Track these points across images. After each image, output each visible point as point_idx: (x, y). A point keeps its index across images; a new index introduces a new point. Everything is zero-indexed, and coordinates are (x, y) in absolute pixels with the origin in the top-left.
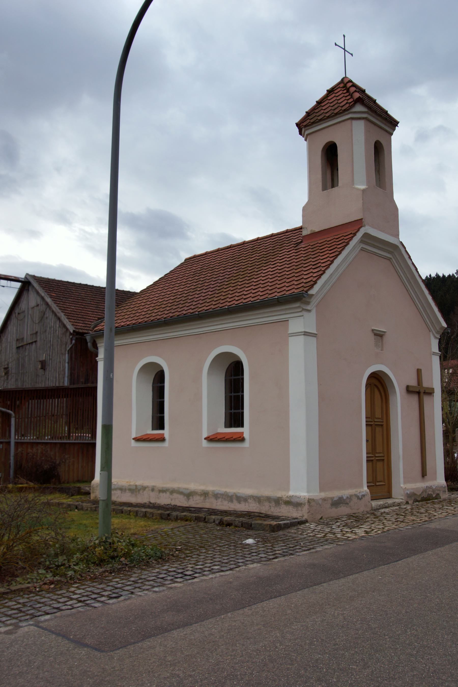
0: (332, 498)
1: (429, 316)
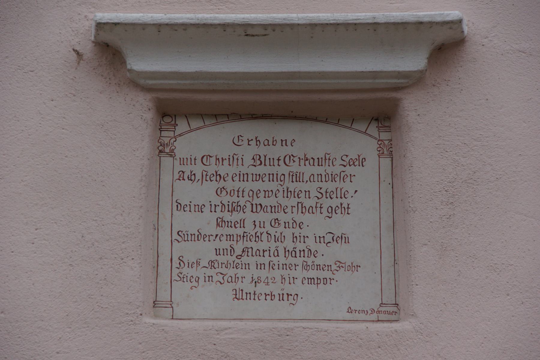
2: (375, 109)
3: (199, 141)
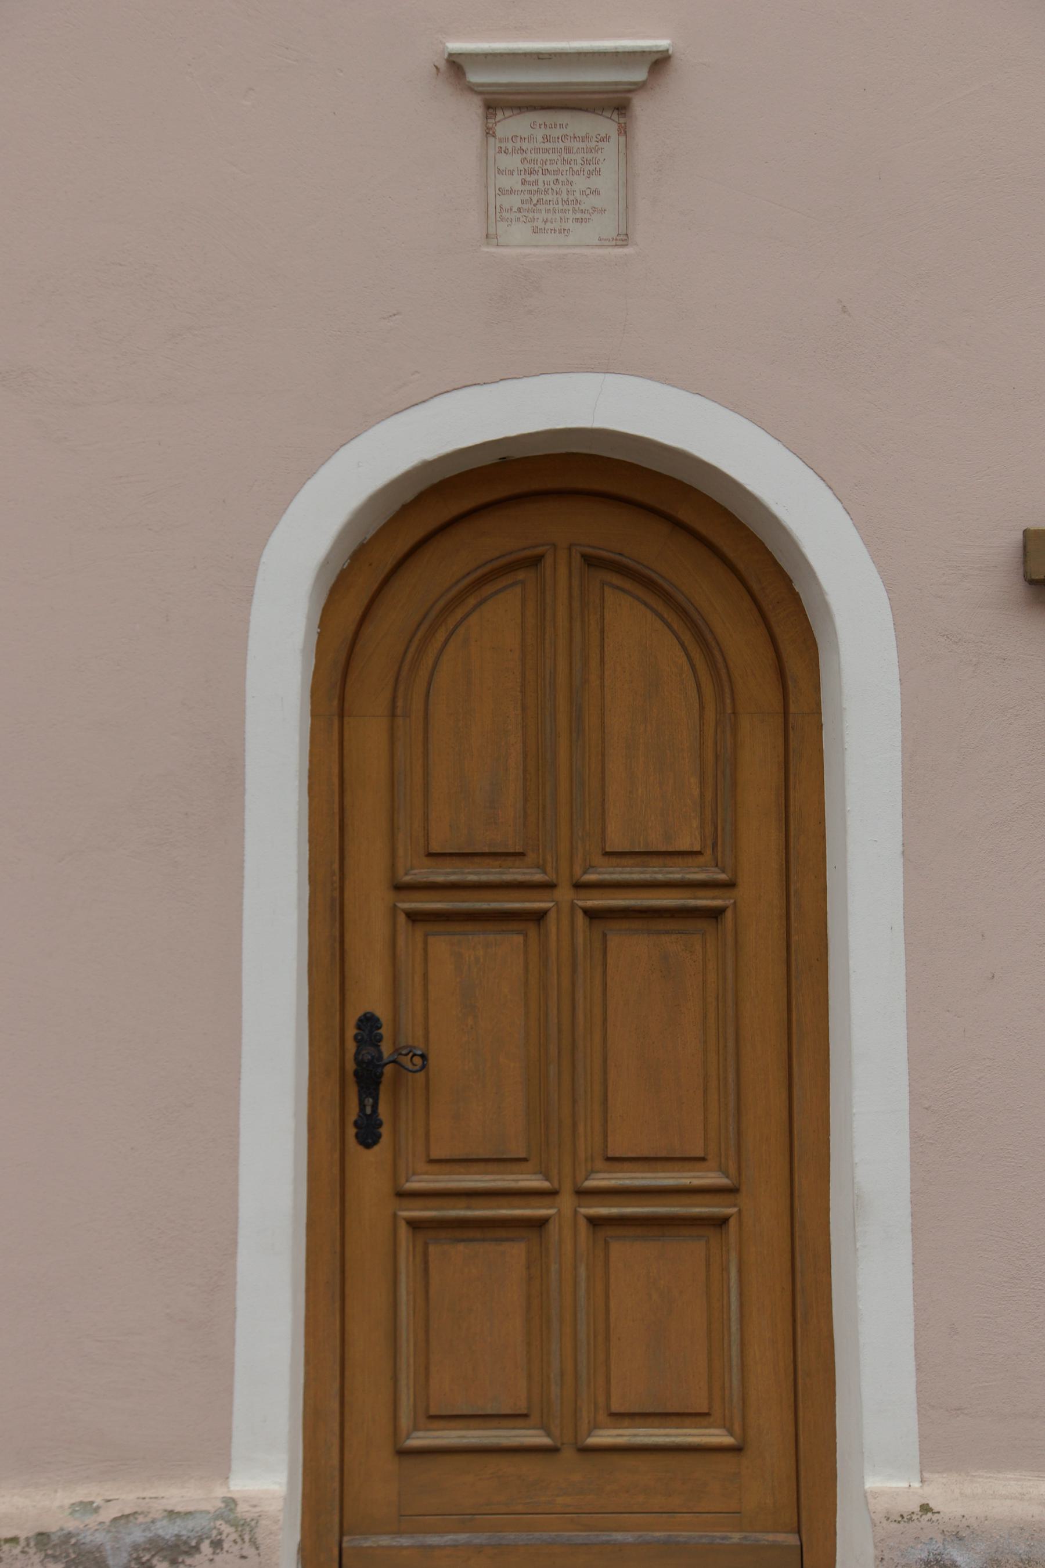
2: (617, 104)
3: (513, 126)
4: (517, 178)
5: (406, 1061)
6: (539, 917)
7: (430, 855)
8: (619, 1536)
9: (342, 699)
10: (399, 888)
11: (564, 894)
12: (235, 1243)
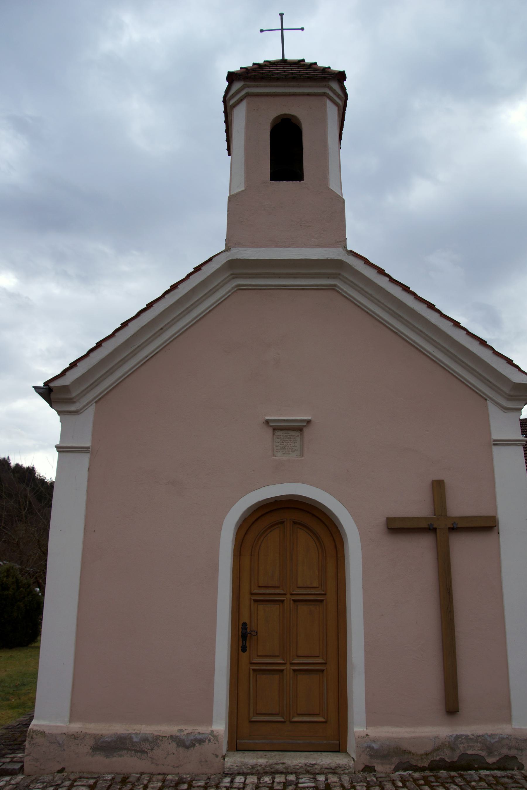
0: (97, 738)
1: (463, 362)
2: (300, 429)
3: (278, 433)
4: (279, 443)
5: (253, 633)
6: (282, 601)
7: (259, 587)
8: (299, 742)
9: (240, 552)
10: (252, 594)
11: (288, 596)
12: (214, 673)
